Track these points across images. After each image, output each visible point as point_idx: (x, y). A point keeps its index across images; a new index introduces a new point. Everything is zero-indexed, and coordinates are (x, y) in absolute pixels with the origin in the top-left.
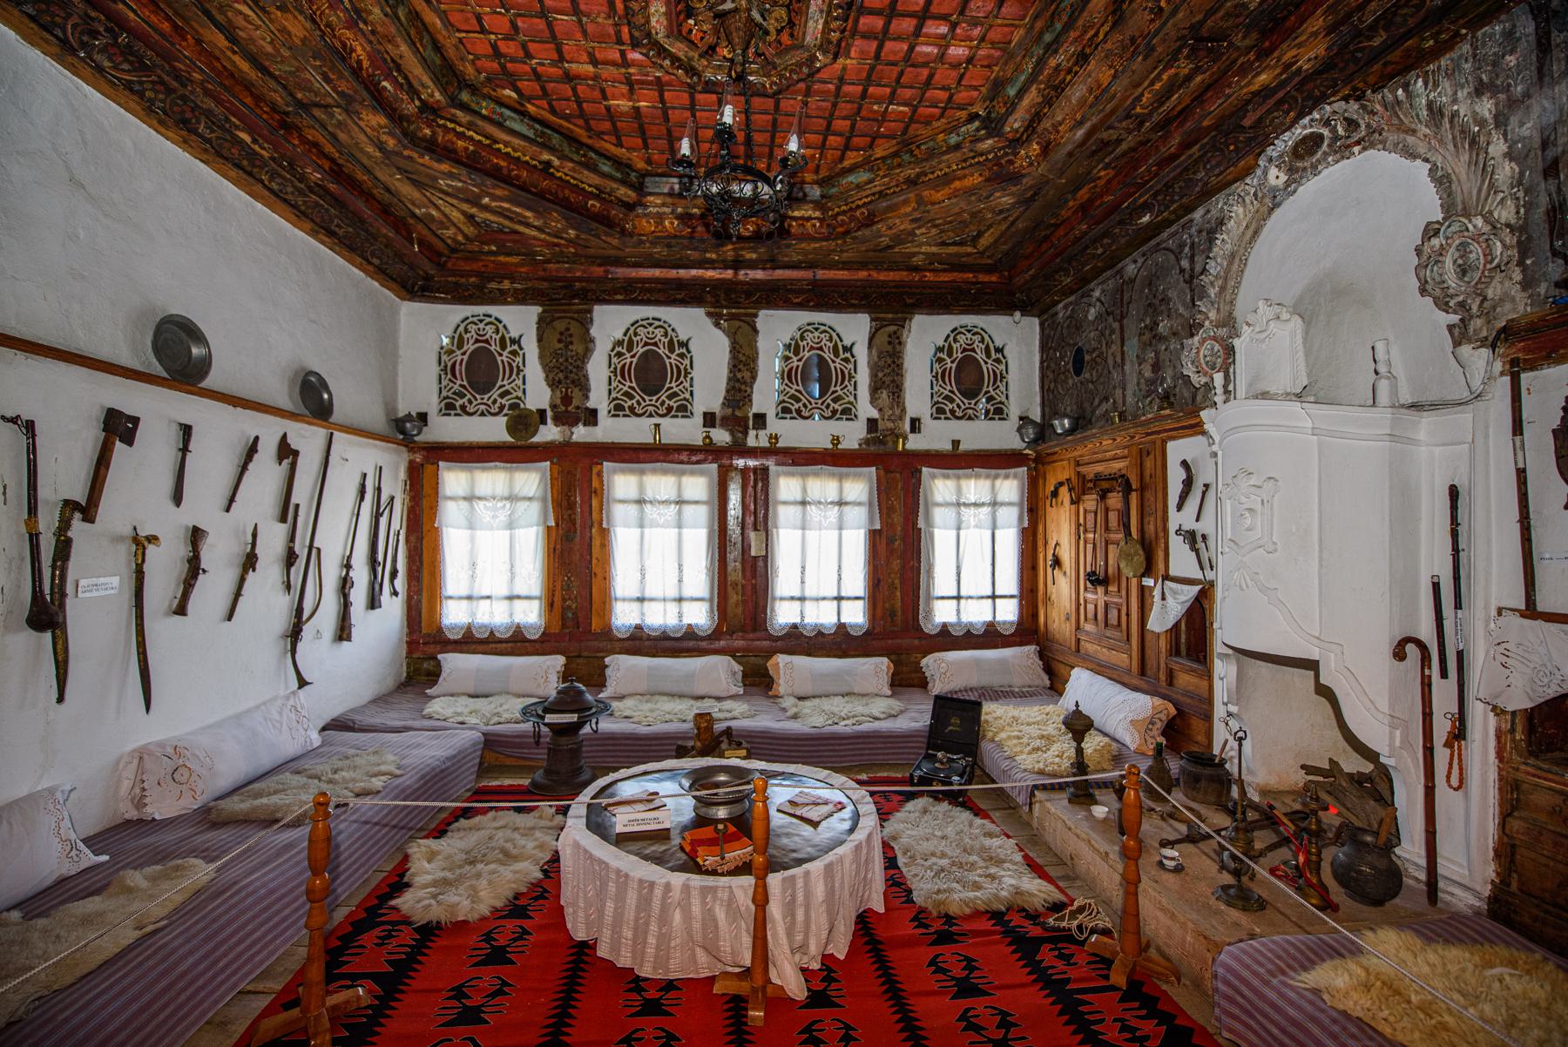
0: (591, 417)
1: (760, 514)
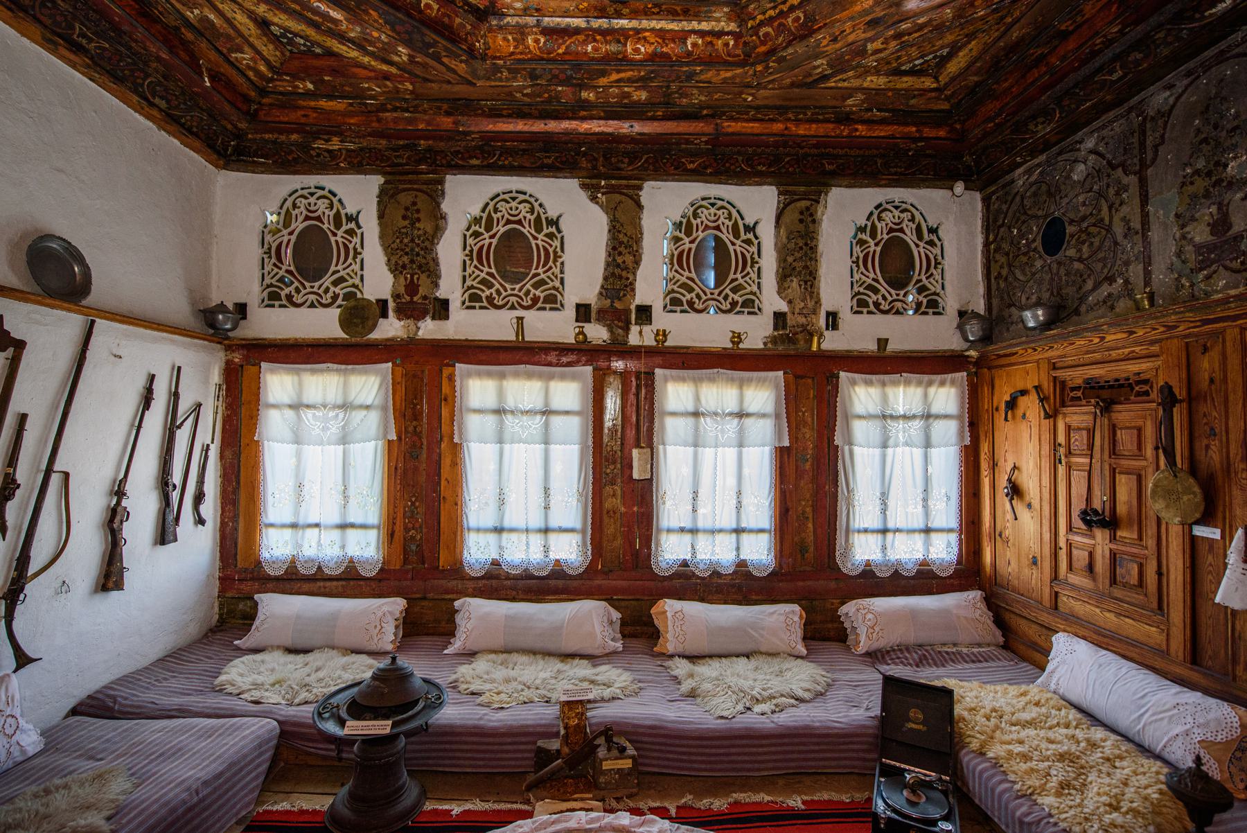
0: (441, 309)
1: (642, 425)
